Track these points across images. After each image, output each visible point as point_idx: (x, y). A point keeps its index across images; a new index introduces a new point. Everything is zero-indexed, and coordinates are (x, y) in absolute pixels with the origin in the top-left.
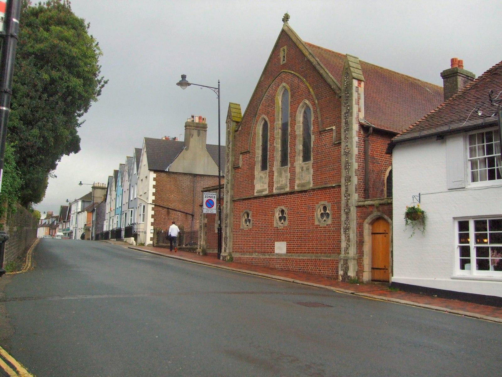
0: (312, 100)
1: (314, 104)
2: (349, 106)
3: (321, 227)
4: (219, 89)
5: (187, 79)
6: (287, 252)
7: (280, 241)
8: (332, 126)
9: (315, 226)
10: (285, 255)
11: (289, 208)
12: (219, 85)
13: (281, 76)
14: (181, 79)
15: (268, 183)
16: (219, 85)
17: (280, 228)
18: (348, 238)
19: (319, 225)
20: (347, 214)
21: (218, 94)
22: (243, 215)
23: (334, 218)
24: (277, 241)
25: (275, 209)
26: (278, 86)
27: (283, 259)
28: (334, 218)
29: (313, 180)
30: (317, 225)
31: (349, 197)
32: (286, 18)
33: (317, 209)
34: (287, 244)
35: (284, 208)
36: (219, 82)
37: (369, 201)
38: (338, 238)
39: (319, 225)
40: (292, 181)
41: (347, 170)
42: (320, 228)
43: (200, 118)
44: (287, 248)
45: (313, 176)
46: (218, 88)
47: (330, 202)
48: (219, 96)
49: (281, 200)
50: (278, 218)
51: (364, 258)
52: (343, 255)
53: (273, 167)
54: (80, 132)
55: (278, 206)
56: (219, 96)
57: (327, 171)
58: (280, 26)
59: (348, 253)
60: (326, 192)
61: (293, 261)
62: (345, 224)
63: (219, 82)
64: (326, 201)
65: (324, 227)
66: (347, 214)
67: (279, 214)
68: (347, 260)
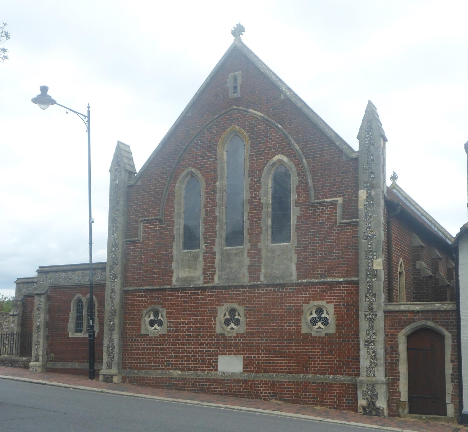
0: (294, 157)
1: (298, 164)
2: (372, 172)
4: (89, 117)
5: (49, 93)
6: (244, 371)
7: (229, 354)
8: (340, 196)
10: (240, 374)
11: (247, 307)
12: (89, 112)
13: (230, 115)
14: (39, 93)
15: (203, 269)
16: (89, 112)
18: (373, 355)
20: (371, 320)
21: (87, 124)
22: (147, 313)
24: (222, 354)
26: (224, 129)
27: (238, 381)
29: (297, 270)
30: (306, 334)
31: (374, 299)
32: (238, 31)
33: (144, 316)
34: (244, 360)
35: (236, 306)
36: (89, 107)
37: (407, 306)
40: (254, 269)
41: (369, 261)
42: (311, 337)
44: (244, 365)
45: (297, 264)
46: (86, 115)
47: (333, 302)
48: (89, 128)
49: (231, 294)
50: (223, 320)
51: (400, 382)
52: (363, 377)
53: (214, 245)
54: (358, 141)
55: (225, 302)
56: (89, 128)
57: (325, 259)
58: (230, 41)
59: (374, 375)
60: (198, 293)
62: (368, 334)
63: (89, 107)
64: (325, 301)
66: (371, 320)
67: (225, 315)
68: (374, 385)
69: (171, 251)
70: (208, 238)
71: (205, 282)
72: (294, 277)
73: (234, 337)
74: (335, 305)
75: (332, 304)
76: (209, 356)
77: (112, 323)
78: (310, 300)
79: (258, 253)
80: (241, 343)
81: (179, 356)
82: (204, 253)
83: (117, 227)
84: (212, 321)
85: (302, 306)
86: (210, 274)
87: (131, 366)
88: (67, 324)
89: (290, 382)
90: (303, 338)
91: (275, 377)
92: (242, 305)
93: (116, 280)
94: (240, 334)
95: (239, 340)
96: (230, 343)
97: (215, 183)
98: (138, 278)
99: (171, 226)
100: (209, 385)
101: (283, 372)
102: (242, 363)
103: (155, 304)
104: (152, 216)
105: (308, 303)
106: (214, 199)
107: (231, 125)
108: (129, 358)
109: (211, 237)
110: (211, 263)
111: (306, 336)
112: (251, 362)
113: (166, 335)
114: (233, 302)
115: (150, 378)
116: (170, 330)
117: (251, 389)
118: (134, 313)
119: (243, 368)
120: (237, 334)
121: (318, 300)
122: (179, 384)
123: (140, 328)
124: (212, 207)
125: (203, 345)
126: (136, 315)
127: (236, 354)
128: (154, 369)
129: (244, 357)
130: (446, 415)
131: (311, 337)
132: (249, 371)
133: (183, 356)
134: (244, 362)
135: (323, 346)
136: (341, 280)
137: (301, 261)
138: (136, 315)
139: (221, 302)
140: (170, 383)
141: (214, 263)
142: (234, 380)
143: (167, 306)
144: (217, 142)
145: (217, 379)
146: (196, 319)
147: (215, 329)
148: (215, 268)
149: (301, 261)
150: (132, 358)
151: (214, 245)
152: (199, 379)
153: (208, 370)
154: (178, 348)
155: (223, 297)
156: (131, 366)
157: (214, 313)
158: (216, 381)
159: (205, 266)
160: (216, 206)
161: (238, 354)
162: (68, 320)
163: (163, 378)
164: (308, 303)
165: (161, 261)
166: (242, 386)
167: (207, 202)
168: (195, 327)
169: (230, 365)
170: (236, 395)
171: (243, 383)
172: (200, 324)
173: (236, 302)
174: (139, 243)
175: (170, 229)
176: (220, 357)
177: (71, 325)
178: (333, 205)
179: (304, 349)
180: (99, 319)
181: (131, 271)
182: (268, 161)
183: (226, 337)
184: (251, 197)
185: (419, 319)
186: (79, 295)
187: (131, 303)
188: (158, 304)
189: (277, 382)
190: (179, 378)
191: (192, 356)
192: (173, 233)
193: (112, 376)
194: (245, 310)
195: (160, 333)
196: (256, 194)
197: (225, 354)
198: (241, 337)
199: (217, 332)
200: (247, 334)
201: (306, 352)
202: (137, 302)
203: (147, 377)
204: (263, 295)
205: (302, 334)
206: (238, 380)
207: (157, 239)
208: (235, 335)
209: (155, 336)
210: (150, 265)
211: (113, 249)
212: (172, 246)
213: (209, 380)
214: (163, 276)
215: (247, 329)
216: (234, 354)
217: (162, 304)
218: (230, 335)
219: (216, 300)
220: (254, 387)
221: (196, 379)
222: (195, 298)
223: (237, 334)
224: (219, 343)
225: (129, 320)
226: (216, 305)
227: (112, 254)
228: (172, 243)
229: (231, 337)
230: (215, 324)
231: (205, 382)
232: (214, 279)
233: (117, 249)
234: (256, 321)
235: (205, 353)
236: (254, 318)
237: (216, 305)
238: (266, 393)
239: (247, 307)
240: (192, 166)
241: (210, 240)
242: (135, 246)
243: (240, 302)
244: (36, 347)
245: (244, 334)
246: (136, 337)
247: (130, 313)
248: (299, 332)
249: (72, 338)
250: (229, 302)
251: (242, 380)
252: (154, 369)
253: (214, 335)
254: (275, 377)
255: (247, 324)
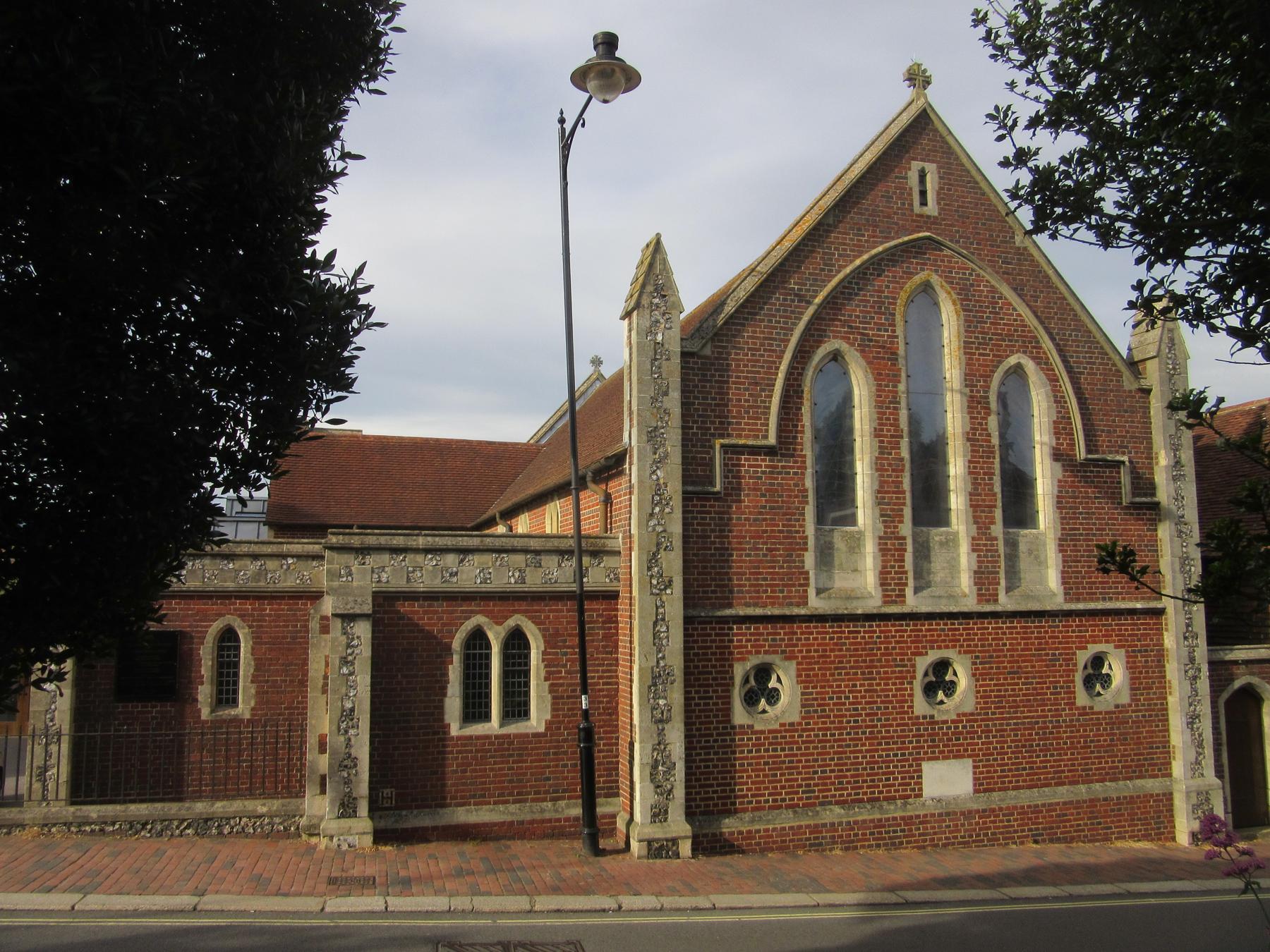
6: (976, 791)
11: (977, 657)
24: (930, 759)
27: (968, 814)
30: (1084, 708)
34: (975, 767)
44: (975, 779)
47: (1123, 646)
55: (932, 648)
69: (802, 526)
70: (888, 504)
71: (885, 603)
72: (1060, 599)
73: (953, 721)
74: (1127, 652)
75: (1123, 650)
76: (903, 766)
78: (1088, 642)
79: (992, 545)
81: (832, 771)
82: (880, 538)
85: (1075, 654)
89: (1065, 803)
90: (1080, 715)
91: (1026, 797)
92: (966, 652)
93: (669, 591)
94: (964, 715)
95: (964, 727)
96: (944, 734)
100: (911, 830)
102: (971, 776)
104: (747, 437)
105: (1086, 648)
107: (923, 270)
108: (701, 786)
109: (895, 504)
110: (896, 561)
111: (1084, 711)
112: (988, 772)
113: (800, 724)
114: (947, 647)
115: (767, 830)
118: (711, 673)
119: (975, 785)
120: (958, 715)
122: (841, 836)
123: (729, 709)
125: (887, 744)
126: (714, 679)
127: (958, 756)
128: (770, 808)
131: (1093, 713)
132: (985, 791)
134: (975, 773)
135: (1112, 729)
138: (714, 679)
139: (925, 647)
140: (817, 838)
141: (903, 561)
142: (963, 813)
143: (797, 658)
144: (894, 298)
145: (925, 816)
146: (870, 685)
147: (912, 707)
148: (906, 573)
149: (1070, 567)
151: (902, 522)
152: (887, 820)
153: (901, 797)
157: (908, 672)
158: (924, 820)
159: (884, 567)
161: (962, 757)
165: (778, 550)
166: (977, 823)
167: (880, 424)
168: (867, 703)
169: (947, 781)
170: (968, 842)
171: (980, 818)
172: (879, 696)
174: (716, 500)
175: (795, 473)
176: (926, 767)
177: (453, 704)
179: (1081, 737)
181: (696, 567)
182: (1000, 362)
183: (937, 723)
184: (972, 429)
185: (1244, 675)
186: (479, 619)
188: (775, 652)
189: (1044, 805)
190: (840, 824)
192: (803, 485)
193: (674, 841)
195: (782, 721)
197: (937, 758)
199: (916, 713)
200: (979, 714)
201: (1085, 742)
202: (717, 647)
203: (758, 831)
205: (1077, 709)
208: (955, 717)
209: (771, 727)
210: (749, 555)
211: (657, 509)
212: (803, 514)
213: (908, 820)
214: (784, 586)
215: (978, 703)
216: (955, 757)
217: (783, 652)
218: (945, 718)
219: (912, 642)
220: (1002, 821)
221: (880, 820)
222: (863, 638)
223: (958, 715)
226: (913, 654)
227: (652, 523)
228: (803, 509)
229: (946, 722)
230: (911, 695)
231: (899, 825)
232: (904, 596)
233: (667, 510)
234: (995, 685)
235: (818, 754)
237: (913, 654)
238: (1023, 831)
239: (977, 657)
240: (843, 338)
241: (892, 510)
242: (705, 506)
243: (962, 646)
245: (972, 714)
247: (700, 673)
248: (1072, 704)
249: (459, 738)
250: (939, 648)
252: (770, 808)
253: (909, 718)
254: (1026, 797)
255: (978, 692)
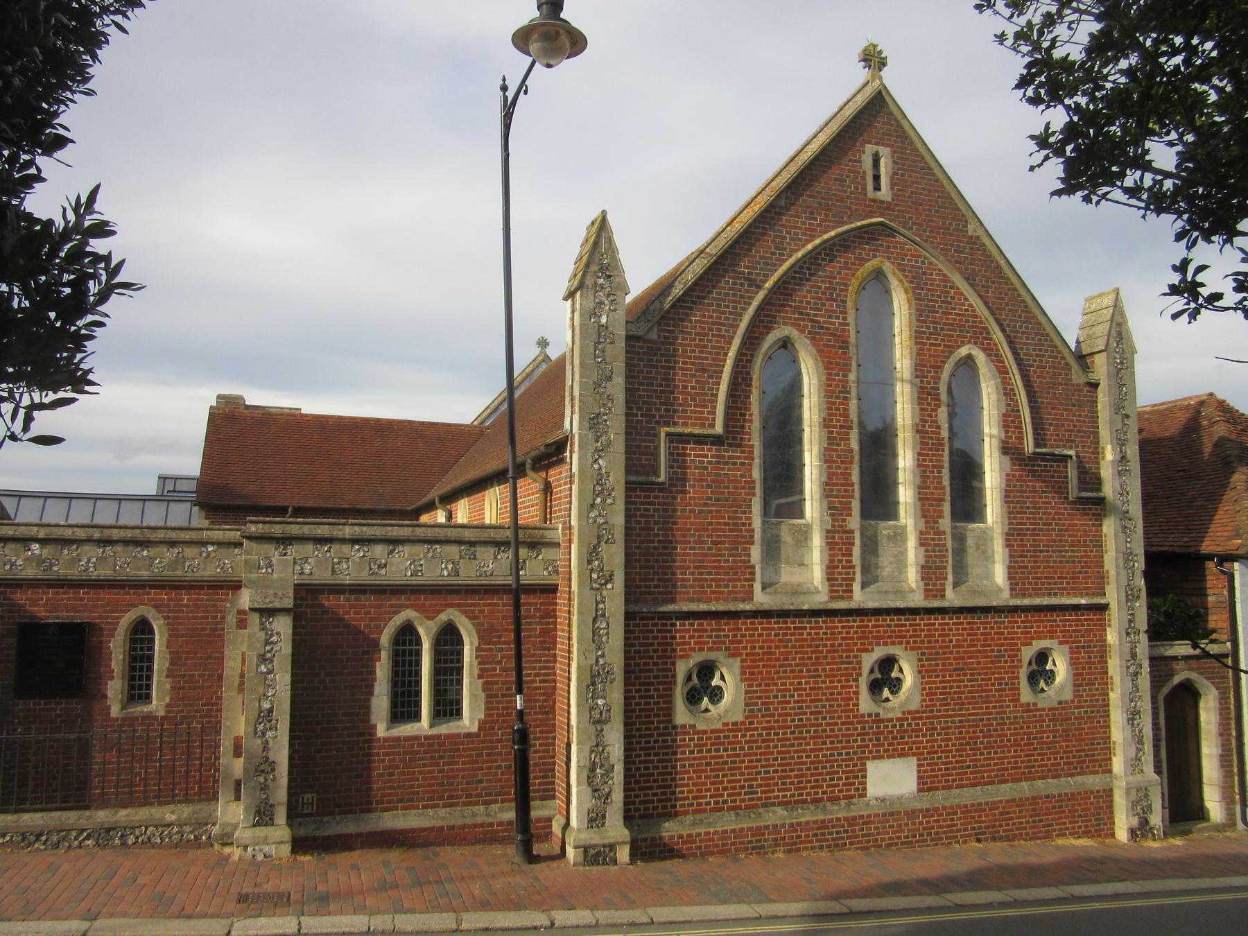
3: (1044, 709)
6: (920, 790)
7: (890, 757)
9: (1022, 705)
17: (890, 716)
19: (1035, 704)
23: (939, 568)
24: (875, 758)
25: (864, 655)
27: (912, 814)
28: (939, 568)
30: (1028, 705)
34: (919, 766)
38: (848, 573)
39: (1035, 704)
43: (1043, 690)
44: (919, 778)
47: (1067, 642)
61: (956, 813)
65: (1050, 709)
70: (836, 497)
72: (1006, 594)
73: (898, 719)
74: (1071, 648)
77: (600, 702)
79: (940, 540)
80: (913, 731)
83: (609, 443)
84: (851, 687)
85: (1019, 650)
86: (843, 579)
87: (646, 809)
88: (368, 700)
92: (912, 649)
93: (609, 586)
94: (910, 712)
95: (909, 725)
96: (889, 732)
97: (846, 375)
98: (658, 580)
99: (746, 458)
101: (992, 783)
102: (915, 773)
103: (710, 649)
104: (693, 425)
105: (1031, 644)
106: (846, 410)
108: (640, 789)
109: (843, 497)
110: (843, 555)
111: (1028, 708)
113: (743, 723)
114: (893, 643)
115: (708, 833)
116: (751, 711)
117: (939, 827)
118: (652, 671)
119: (919, 784)
120: (904, 713)
121: (1045, 638)
124: (841, 427)
125: (831, 743)
126: (656, 677)
129: (919, 760)
130: (1208, 820)
132: (929, 790)
133: (785, 771)
134: (919, 772)
136: (1083, 601)
137: (1016, 562)
138: (655, 677)
141: (851, 555)
142: (906, 813)
145: (869, 816)
147: (857, 705)
148: (853, 567)
149: (1016, 562)
150: (651, 788)
151: (850, 515)
153: (845, 797)
154: (772, 753)
155: (871, 632)
156: (646, 809)
157: (854, 669)
159: (831, 561)
160: (851, 428)
161: (906, 755)
162: (372, 686)
163: (742, 830)
164: (1031, 644)
166: (921, 823)
167: (829, 415)
168: (812, 701)
170: (911, 843)
171: (924, 817)
172: (824, 694)
173: (901, 643)
174: (660, 490)
175: (742, 464)
176: (871, 766)
177: (380, 702)
178: (1061, 461)
180: (485, 683)
182: (951, 353)
183: (882, 721)
187: (641, 645)
188: (719, 649)
189: (987, 803)
190: (783, 825)
191: (808, 769)
192: (751, 476)
193: (612, 847)
194: (920, 660)
195: (725, 720)
196: (930, 416)
197: (881, 757)
198: (913, 719)
200: (924, 712)
201: (1029, 739)
203: (699, 835)
204: (951, 630)
206: (914, 811)
207: (709, 486)
208: (900, 715)
209: (713, 727)
211: (599, 500)
213: (852, 821)
216: (900, 756)
217: (727, 649)
220: (945, 820)
223: (904, 713)
224: (867, 734)
225: (637, 691)
229: (891, 720)
230: (857, 693)
232: (851, 591)
233: (609, 501)
234: (941, 682)
236: (937, 676)
239: (923, 654)
240: (792, 325)
241: (841, 503)
243: (908, 642)
244: (262, 780)
245: (918, 712)
246: (659, 735)
247: (640, 671)
250: (886, 644)
251: (921, 811)
253: (855, 717)
255: (924, 689)
